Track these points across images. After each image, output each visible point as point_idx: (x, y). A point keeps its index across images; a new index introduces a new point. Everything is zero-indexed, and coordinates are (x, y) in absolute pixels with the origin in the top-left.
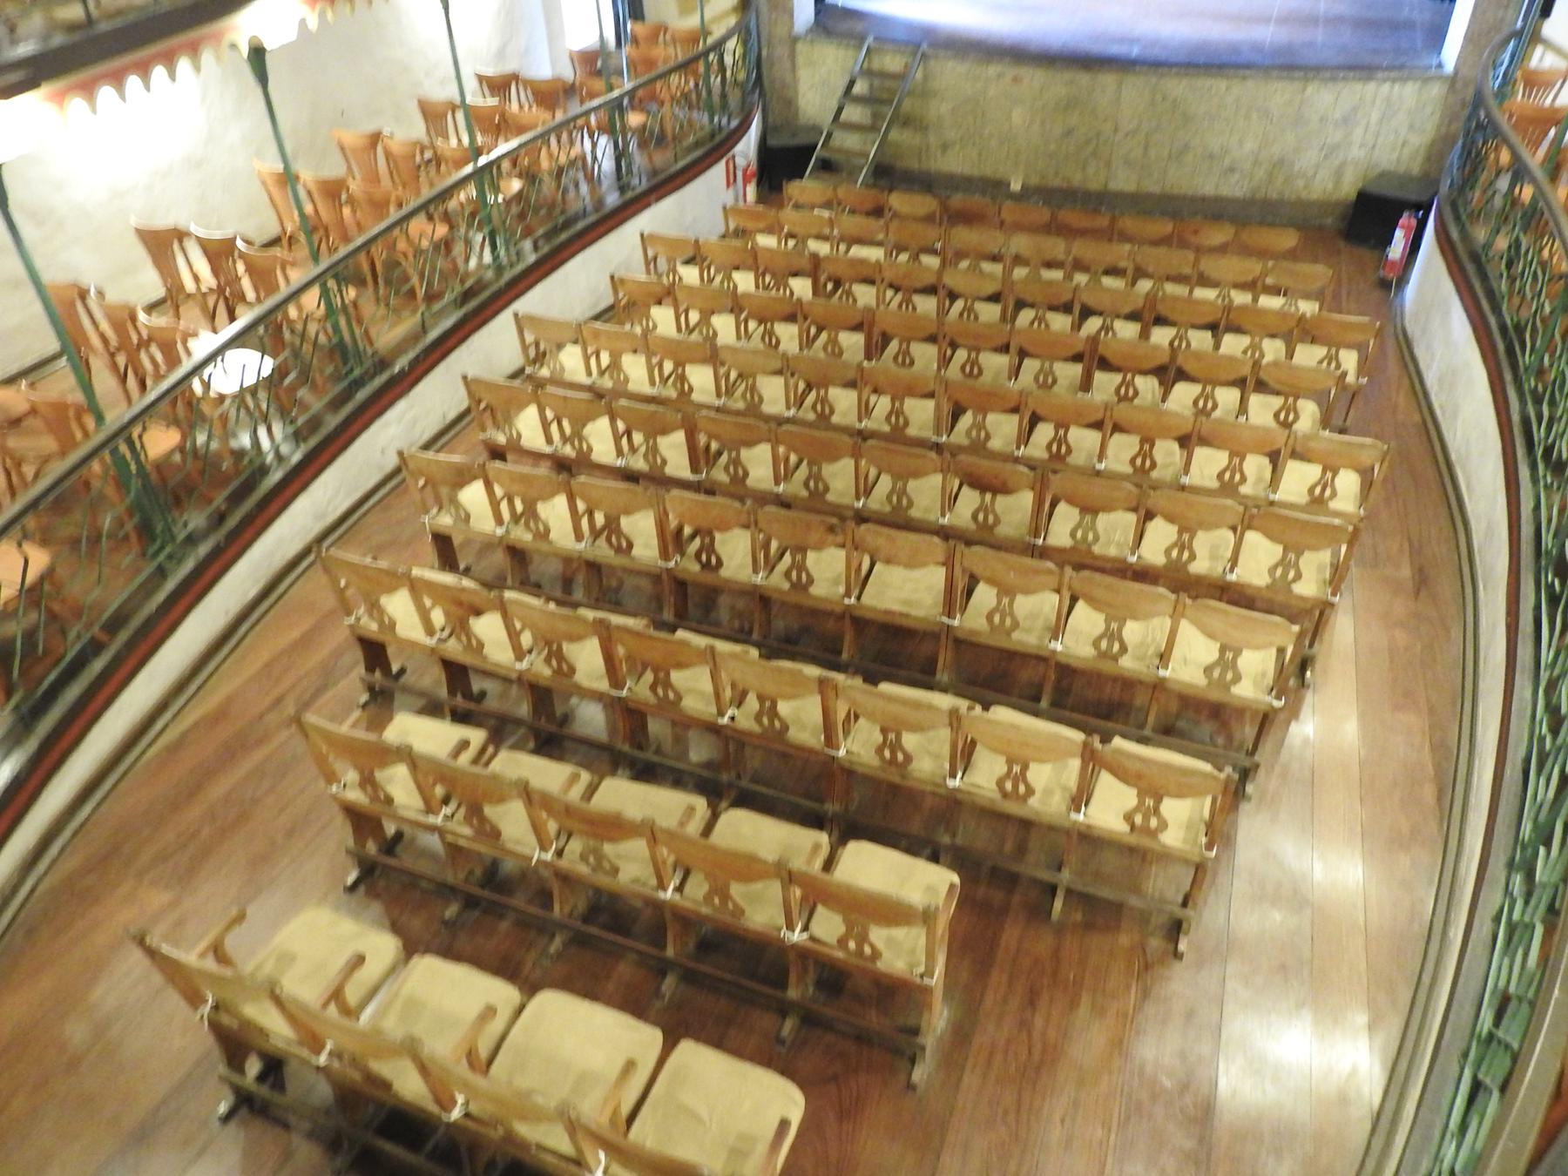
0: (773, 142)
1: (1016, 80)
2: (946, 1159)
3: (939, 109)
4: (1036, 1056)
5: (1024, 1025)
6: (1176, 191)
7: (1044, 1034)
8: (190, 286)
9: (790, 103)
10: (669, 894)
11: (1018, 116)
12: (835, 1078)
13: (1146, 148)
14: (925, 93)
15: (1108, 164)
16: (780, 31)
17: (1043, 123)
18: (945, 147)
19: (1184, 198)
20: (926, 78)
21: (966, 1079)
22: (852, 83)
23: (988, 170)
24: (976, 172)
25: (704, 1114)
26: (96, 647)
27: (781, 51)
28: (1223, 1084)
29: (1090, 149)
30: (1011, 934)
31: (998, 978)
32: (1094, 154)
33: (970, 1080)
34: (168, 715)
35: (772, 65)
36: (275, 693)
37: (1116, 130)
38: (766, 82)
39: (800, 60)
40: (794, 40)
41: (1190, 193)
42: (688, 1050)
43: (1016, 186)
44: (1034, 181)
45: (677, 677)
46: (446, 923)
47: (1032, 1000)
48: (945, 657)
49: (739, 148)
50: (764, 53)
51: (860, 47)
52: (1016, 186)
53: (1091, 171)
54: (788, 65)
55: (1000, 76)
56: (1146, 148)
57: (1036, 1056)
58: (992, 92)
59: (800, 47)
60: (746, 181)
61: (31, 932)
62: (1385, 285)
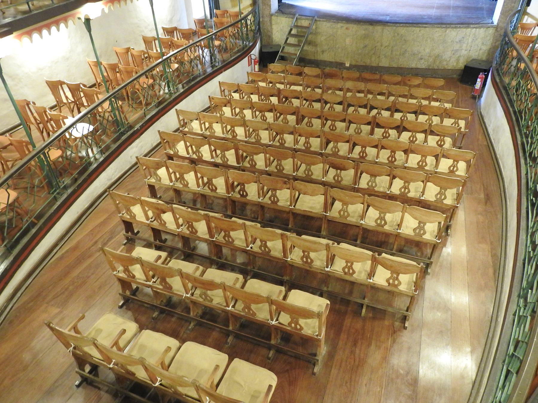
0: (263, 50)
1: (347, 28)
2: (326, 398)
3: (321, 39)
4: (357, 363)
5: (352, 352)
6: (402, 66)
8: (65, 101)
9: (270, 37)
11: (348, 41)
13: (392, 51)
16: (266, 12)
17: (356, 43)
18: (323, 52)
20: (316, 28)
22: (291, 30)
26: (33, 225)
27: (267, 19)
29: (373, 52)
30: (348, 321)
31: (343, 336)
33: (334, 371)
35: (264, 24)
37: (381, 46)
39: (273, 22)
41: (407, 67)
43: (347, 65)
44: (354, 63)
46: (153, 318)
47: (355, 344)
48: (324, 226)
50: (261, 20)
52: (347, 65)
53: (373, 59)
54: (269, 24)
57: (357, 363)
60: (255, 64)
61: (11, 322)
62: (474, 98)
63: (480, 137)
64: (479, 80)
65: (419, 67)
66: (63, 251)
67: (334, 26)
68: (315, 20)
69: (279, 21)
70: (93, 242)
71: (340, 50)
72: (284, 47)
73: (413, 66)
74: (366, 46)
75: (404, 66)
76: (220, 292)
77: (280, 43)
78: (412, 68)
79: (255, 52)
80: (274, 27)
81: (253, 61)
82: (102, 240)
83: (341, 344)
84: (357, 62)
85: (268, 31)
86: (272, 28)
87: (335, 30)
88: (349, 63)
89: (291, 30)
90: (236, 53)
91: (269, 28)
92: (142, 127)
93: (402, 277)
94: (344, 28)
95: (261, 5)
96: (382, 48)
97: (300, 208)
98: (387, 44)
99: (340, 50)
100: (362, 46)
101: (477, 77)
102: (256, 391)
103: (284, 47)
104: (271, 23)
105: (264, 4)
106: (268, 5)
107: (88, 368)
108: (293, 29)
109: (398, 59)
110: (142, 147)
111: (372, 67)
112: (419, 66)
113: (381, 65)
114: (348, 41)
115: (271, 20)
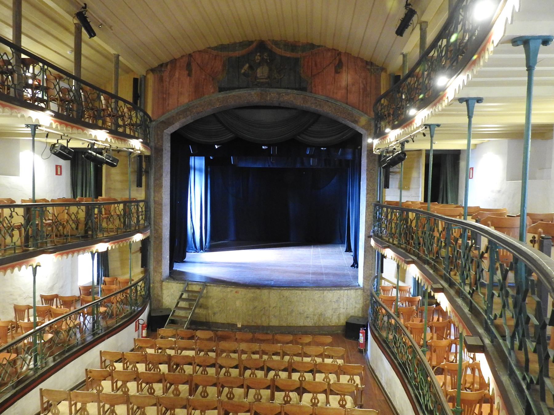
0: (153, 314)
1: (236, 292)
3: (212, 302)
6: (291, 325)
9: (160, 301)
11: (238, 303)
13: (280, 311)
15: (269, 317)
17: (246, 305)
18: (214, 314)
20: (207, 292)
22: (178, 303)
35: (154, 289)
37: (270, 307)
39: (164, 288)
41: (296, 325)
44: (245, 324)
50: (151, 286)
53: (263, 319)
55: (231, 291)
60: (143, 329)
62: (361, 351)
64: (361, 335)
71: (231, 312)
72: (174, 311)
73: (301, 324)
74: (255, 308)
77: (170, 307)
79: (144, 317)
80: (165, 292)
85: (158, 296)
87: (225, 294)
91: (160, 293)
94: (234, 292)
98: (274, 305)
99: (231, 312)
100: (251, 307)
101: (359, 333)
105: (155, 271)
106: (159, 272)
111: (263, 326)
112: (306, 324)
113: (271, 324)
114: (238, 303)
115: (161, 286)
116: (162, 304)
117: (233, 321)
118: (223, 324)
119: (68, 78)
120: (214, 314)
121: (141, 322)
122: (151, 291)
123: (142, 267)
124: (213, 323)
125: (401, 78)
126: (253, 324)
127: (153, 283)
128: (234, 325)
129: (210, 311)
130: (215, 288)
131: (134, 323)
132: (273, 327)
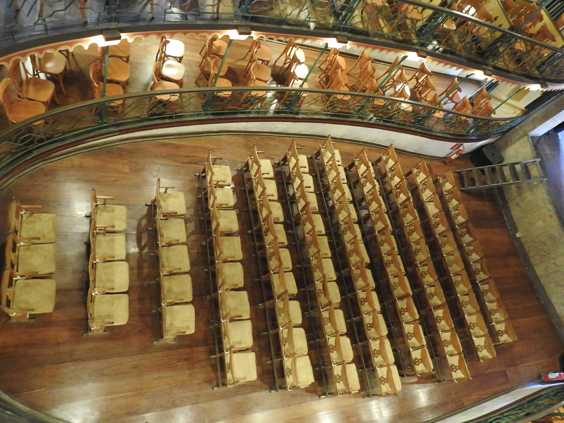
0: (484, 150)
1: (551, 216)
2: (139, 356)
3: (528, 196)
4: (172, 366)
5: (179, 360)
6: (546, 290)
7: (178, 366)
8: (288, 54)
9: (506, 145)
10: (267, 247)
11: (540, 223)
12: (148, 326)
13: (554, 272)
14: (531, 188)
15: (541, 262)
16: (527, 129)
17: (543, 233)
18: (518, 205)
19: (546, 294)
20: (536, 186)
21: (159, 353)
22: (518, 163)
23: (518, 223)
24: (515, 219)
25: (115, 306)
26: (171, 118)
27: (521, 133)
28: (254, 415)
29: (544, 254)
30: (202, 349)
31: (188, 350)
32: (542, 256)
33: (160, 354)
34: (172, 137)
35: (515, 132)
36: (190, 154)
37: (554, 259)
38: (507, 134)
39: (521, 140)
40: (526, 134)
41: (549, 295)
42: (125, 298)
43: (518, 235)
44: (523, 240)
45: (374, 202)
46: (147, 229)
47: (186, 359)
48: (445, 278)
49: (465, 144)
50: (517, 128)
51: (535, 158)
52: (518, 235)
53: (536, 257)
54: (518, 137)
55: (549, 210)
56: (554, 272)
57: (172, 366)
58: (543, 210)
59: (526, 138)
60: (456, 153)
61: (108, 152)
62: (540, 377)
63: (473, 397)
64: (557, 374)
65: (555, 307)
66: (172, 142)
67: (547, 202)
68: (542, 181)
69: (524, 145)
70: (188, 154)
71: (527, 220)
72: (506, 165)
73: (554, 301)
74: (544, 244)
75: (547, 292)
76: (310, 227)
77: (505, 158)
78: (550, 301)
79: (469, 147)
80: (518, 144)
81: (457, 150)
82: (193, 159)
83: (182, 351)
84: (526, 242)
85: (511, 140)
86: (515, 142)
87: (543, 205)
88: (521, 235)
89: (518, 163)
90: (450, 134)
91: (514, 140)
92: (302, 118)
93: (459, 372)
94: (550, 213)
95: (530, 119)
96: (551, 261)
97: (274, 278)
98: (558, 263)
99: (527, 220)
100: (543, 239)
101: (560, 372)
102: (113, 315)
103: (506, 165)
104: (519, 139)
105: (533, 121)
106: (534, 125)
107: (203, 174)
108: (519, 165)
109: (550, 283)
110: (291, 128)
111: (529, 260)
112: (556, 307)
113: (535, 267)
114: (540, 223)
115: (522, 137)
116: (506, 149)
117: (520, 228)
118: (512, 218)
119: (416, 7)
120: (518, 205)
121: (461, 148)
122: (512, 131)
123: (526, 108)
124: (508, 208)
125: (90, 334)
126: (527, 248)
127: (521, 127)
128: (516, 230)
129: (518, 199)
130: (545, 191)
131: (456, 143)
132: (534, 270)
